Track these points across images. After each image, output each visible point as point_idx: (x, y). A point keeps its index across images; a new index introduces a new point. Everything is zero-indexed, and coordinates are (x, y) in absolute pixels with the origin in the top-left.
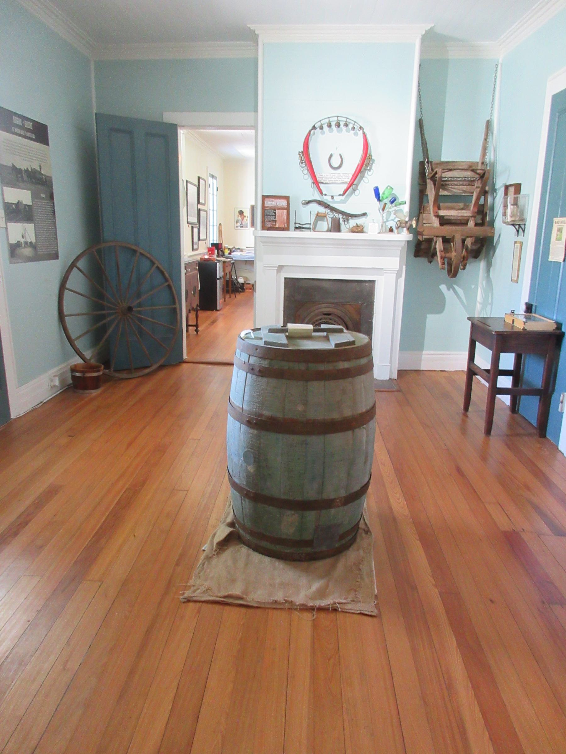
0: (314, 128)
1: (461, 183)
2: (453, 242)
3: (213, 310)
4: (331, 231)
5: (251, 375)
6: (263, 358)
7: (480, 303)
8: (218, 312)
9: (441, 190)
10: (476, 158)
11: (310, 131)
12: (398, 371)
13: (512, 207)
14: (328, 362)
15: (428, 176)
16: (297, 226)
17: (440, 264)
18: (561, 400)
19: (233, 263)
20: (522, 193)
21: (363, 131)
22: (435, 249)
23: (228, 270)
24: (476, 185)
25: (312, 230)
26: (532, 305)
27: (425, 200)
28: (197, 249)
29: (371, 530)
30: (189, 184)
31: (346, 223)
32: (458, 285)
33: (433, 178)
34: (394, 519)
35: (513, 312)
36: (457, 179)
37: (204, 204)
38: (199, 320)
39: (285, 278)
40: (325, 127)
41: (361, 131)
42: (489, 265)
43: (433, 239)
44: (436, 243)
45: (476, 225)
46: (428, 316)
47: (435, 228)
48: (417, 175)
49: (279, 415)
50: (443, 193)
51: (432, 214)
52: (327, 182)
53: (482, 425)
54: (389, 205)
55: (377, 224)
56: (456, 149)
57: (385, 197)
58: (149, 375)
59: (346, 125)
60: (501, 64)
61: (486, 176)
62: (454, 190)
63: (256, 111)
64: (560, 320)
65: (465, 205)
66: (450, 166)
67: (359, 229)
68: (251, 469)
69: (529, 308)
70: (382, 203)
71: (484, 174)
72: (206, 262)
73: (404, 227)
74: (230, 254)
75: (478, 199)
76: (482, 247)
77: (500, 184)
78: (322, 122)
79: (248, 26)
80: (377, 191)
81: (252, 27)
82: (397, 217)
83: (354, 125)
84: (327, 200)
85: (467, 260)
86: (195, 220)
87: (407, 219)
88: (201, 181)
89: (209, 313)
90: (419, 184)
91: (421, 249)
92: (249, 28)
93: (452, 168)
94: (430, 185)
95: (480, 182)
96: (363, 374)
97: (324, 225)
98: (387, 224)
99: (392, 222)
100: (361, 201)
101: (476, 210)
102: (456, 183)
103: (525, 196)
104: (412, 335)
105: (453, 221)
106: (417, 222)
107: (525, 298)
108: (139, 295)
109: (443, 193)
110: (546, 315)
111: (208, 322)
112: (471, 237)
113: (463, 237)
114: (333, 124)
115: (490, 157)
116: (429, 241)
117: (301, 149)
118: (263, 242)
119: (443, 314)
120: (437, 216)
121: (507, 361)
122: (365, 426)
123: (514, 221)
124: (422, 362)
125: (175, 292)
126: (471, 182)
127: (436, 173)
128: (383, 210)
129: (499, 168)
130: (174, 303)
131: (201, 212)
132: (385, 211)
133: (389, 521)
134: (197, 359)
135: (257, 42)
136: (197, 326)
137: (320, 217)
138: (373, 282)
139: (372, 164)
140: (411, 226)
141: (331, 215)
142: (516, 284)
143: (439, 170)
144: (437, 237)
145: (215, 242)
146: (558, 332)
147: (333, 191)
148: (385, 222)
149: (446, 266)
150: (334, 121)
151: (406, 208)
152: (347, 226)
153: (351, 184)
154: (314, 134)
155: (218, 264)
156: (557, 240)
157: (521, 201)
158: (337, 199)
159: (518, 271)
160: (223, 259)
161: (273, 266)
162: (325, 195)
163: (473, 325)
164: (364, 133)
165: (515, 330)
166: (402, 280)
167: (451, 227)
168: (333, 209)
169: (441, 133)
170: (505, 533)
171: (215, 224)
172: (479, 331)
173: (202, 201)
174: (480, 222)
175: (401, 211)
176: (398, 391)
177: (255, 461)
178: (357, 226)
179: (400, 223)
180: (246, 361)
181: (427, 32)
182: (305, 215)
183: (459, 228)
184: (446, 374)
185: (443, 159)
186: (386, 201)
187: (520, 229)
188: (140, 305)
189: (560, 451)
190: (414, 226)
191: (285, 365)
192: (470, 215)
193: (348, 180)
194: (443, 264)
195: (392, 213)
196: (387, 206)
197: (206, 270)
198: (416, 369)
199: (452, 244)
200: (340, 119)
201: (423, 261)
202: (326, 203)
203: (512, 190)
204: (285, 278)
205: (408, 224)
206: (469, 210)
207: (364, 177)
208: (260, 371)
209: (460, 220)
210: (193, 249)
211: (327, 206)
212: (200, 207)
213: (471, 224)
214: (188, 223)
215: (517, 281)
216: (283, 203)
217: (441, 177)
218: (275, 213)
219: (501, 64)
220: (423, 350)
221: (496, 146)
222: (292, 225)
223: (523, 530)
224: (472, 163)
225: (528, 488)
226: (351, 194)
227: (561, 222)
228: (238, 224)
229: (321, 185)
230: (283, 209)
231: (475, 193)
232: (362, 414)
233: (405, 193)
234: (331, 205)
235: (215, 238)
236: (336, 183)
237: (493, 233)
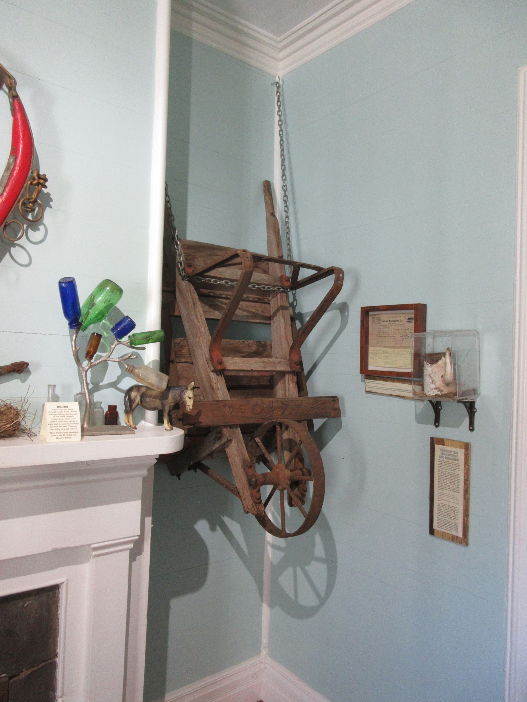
15: (188, 268)
20: (427, 331)
32: (231, 517)
44: (229, 441)
57: (93, 313)
80: (68, 291)
98: (98, 397)
99: (111, 390)
105: (245, 382)
120: (221, 371)
128: (90, 355)
138: (51, 593)
140: (179, 405)
144: (231, 427)
151: (151, 353)
159: (466, 514)
190: (189, 403)
192: (288, 369)
205: (170, 400)
209: (257, 378)
215: (464, 540)
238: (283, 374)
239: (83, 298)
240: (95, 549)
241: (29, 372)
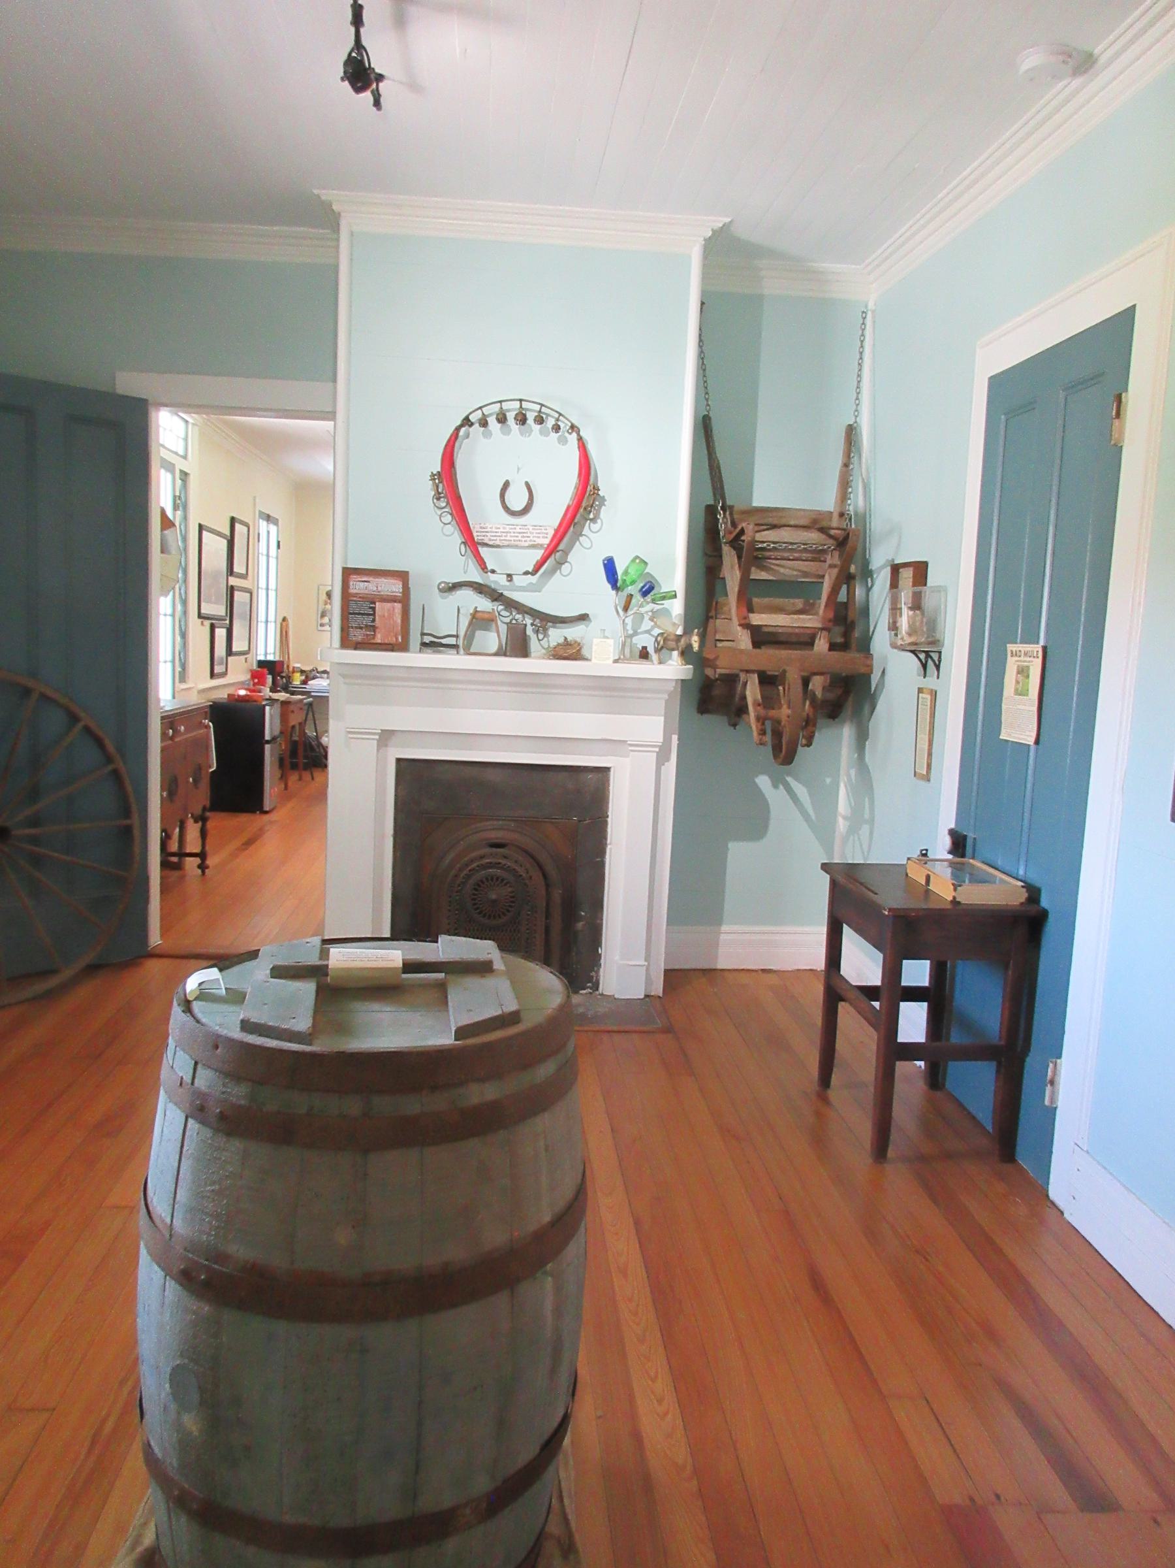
0: (467, 422)
1: (796, 555)
2: (783, 684)
3: (253, 812)
4: (505, 655)
5: (197, 1126)
6: (232, 1074)
7: (845, 818)
8: (266, 818)
9: (753, 569)
10: (827, 502)
11: (458, 429)
12: (668, 973)
13: (911, 613)
14: (434, 1088)
15: (722, 535)
16: (427, 639)
17: (755, 734)
18: (1049, 1077)
19: (310, 705)
20: (929, 584)
22: (744, 698)
23: (295, 719)
24: (829, 562)
25: (462, 651)
26: (965, 837)
27: (718, 587)
28: (224, 674)
29: (579, 1546)
30: (205, 533)
31: (541, 636)
32: (796, 779)
33: (736, 543)
34: (647, 1484)
35: (925, 855)
36: (790, 547)
37: (244, 576)
38: (208, 841)
39: (399, 760)
40: (492, 421)
41: (574, 435)
42: (862, 737)
43: (737, 676)
44: (745, 684)
45: (833, 647)
46: (730, 845)
47: (742, 651)
48: (700, 534)
49: (278, 1261)
50: (757, 574)
51: (735, 621)
52: (498, 543)
53: (865, 1129)
54: (638, 598)
55: (611, 642)
56: (782, 481)
58: (49, 996)
59: (540, 420)
60: (873, 312)
61: (850, 543)
62: (782, 570)
63: (335, 380)
64: (1035, 878)
65: (806, 603)
66: (771, 519)
67: (570, 652)
68: (191, 1423)
69: (959, 844)
70: (624, 594)
71: (847, 538)
72: (239, 704)
73: (673, 650)
74: (305, 682)
75: (835, 591)
76: (848, 695)
77: (880, 558)
78: (486, 411)
79: (316, 192)
80: (610, 567)
81: (326, 195)
82: (656, 626)
83: (558, 420)
84: (496, 582)
85: (814, 725)
86: (221, 610)
87: (679, 632)
88: (237, 526)
89: (243, 818)
90: (706, 554)
91: (712, 695)
92: (318, 196)
93: (776, 522)
94: (729, 556)
95: (836, 554)
96: (544, 1110)
97: (491, 640)
98: (635, 640)
100: (576, 587)
101: (831, 615)
103: (939, 589)
104: (696, 887)
105: (782, 639)
106: (703, 637)
107: (948, 819)
108: (34, 794)
109: (757, 574)
110: (999, 863)
111: (236, 843)
112: (821, 674)
113: (805, 674)
114: (511, 416)
115: (857, 501)
116: (731, 680)
117: (437, 468)
118: (344, 676)
119: (765, 840)
120: (747, 626)
121: (917, 973)
122: (549, 1266)
123: (916, 644)
124: (721, 950)
125: (129, 788)
126: (818, 555)
127: (742, 532)
128: (626, 609)
129: (876, 525)
130: (126, 812)
131: (236, 593)
132: (630, 612)
133: (632, 1488)
134: (188, 943)
135: (336, 228)
136: (202, 855)
137: (480, 621)
138: (606, 770)
139: (600, 507)
140: (690, 646)
141: (506, 617)
142: (922, 783)
143: (749, 528)
144: (747, 671)
145: (270, 658)
146: (1032, 909)
147: (512, 563)
148: (631, 636)
149: (768, 738)
150: (512, 408)
151: (677, 607)
152: (544, 643)
153: (551, 550)
154: (467, 436)
155: (267, 708)
156: (1017, 693)
157: (929, 601)
158: (519, 580)
159: (930, 754)
160: (282, 696)
161: (379, 727)
162: (493, 572)
163: (834, 884)
164: (580, 439)
165: (933, 905)
166: (671, 767)
167: (777, 652)
168: (511, 605)
169: (750, 447)
170: (949, 1512)
171: (272, 617)
172: (851, 899)
173: (238, 568)
174: (840, 640)
175: (666, 612)
176: (668, 1030)
177: (202, 1403)
178: (567, 644)
179: (665, 640)
180: (188, 1079)
181: (717, 234)
182: (447, 615)
183: (795, 654)
184: (772, 980)
185: (756, 503)
186: (631, 589)
187: (930, 661)
188: (34, 822)
189: (1053, 1203)
190: (696, 646)
191: (300, 1103)
192: (820, 625)
193: (547, 541)
194: (763, 732)
195: (647, 618)
196: (633, 601)
197: (234, 723)
198: (706, 966)
199: (781, 688)
200: (525, 405)
201: (716, 723)
202: (494, 591)
203: (907, 575)
204: (399, 760)
206: (816, 614)
207: (581, 535)
208: (222, 1117)
210: (212, 675)
211: (496, 596)
212: (233, 581)
213: (821, 645)
214: (200, 616)
215: (927, 778)
216: (395, 587)
217: (754, 541)
218: (374, 609)
219: (873, 312)
220: (720, 924)
221: (869, 478)
222: (415, 640)
223: (998, 1497)
224: (819, 513)
225: (991, 1333)
226: (552, 572)
227: (1026, 654)
228: (326, 620)
229: (483, 551)
230: (393, 600)
231: (827, 577)
232: (539, 1236)
233: (674, 575)
234: (506, 593)
235: (271, 649)
236: (516, 547)
237: (870, 667)
240: (631, 745)
241: (590, 620)
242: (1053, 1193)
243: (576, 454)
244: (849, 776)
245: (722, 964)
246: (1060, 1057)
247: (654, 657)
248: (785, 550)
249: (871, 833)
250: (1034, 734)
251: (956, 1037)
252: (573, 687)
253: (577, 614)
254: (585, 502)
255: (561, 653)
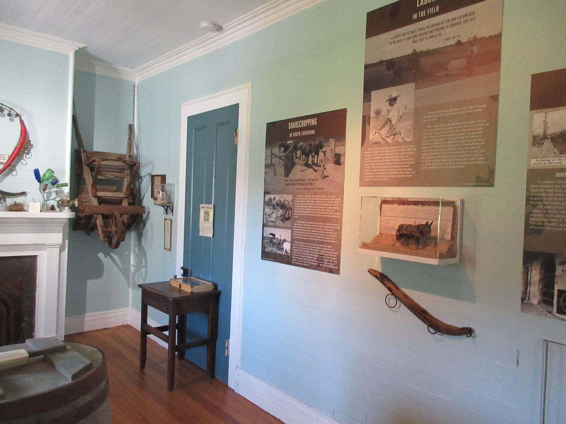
7: (133, 266)
10: (123, 150)
12: (65, 336)
21: (20, 118)
36: (110, 167)
41: (18, 118)
42: (140, 236)
44: (96, 219)
45: (130, 204)
57: (45, 178)
64: (215, 281)
65: (118, 188)
66: (103, 156)
70: (43, 185)
76: (136, 221)
77: (144, 172)
80: (37, 173)
91: (80, 225)
93: (105, 158)
95: (129, 170)
98: (48, 202)
99: (53, 201)
101: (128, 193)
102: (109, 170)
104: (75, 300)
107: (180, 262)
116: (89, 217)
120: (96, 196)
126: (121, 170)
128: (44, 190)
129: (142, 161)
140: (74, 205)
142: (169, 252)
144: (97, 214)
151: (67, 190)
157: (167, 188)
159: (171, 241)
166: (66, 253)
172: (151, 297)
174: (131, 201)
178: (16, 204)
181: (80, 49)
185: (95, 149)
189: (230, 388)
190: (77, 205)
193: (5, 161)
198: (80, 331)
201: (81, 234)
203: (158, 181)
205: (71, 203)
207: (22, 159)
209: (116, 200)
213: (125, 203)
215: (170, 250)
220: (84, 313)
221: (138, 143)
224: (121, 155)
233: (66, 177)
238: (124, 198)
239: (41, 174)
242: (230, 385)
243: (19, 127)
244: (135, 251)
245: (86, 330)
246: (229, 338)
247: (57, 209)
248: (110, 168)
249: (146, 271)
250: (212, 234)
251: (188, 340)
252: (18, 223)
253: (20, 192)
254: (24, 146)
255: (14, 208)
